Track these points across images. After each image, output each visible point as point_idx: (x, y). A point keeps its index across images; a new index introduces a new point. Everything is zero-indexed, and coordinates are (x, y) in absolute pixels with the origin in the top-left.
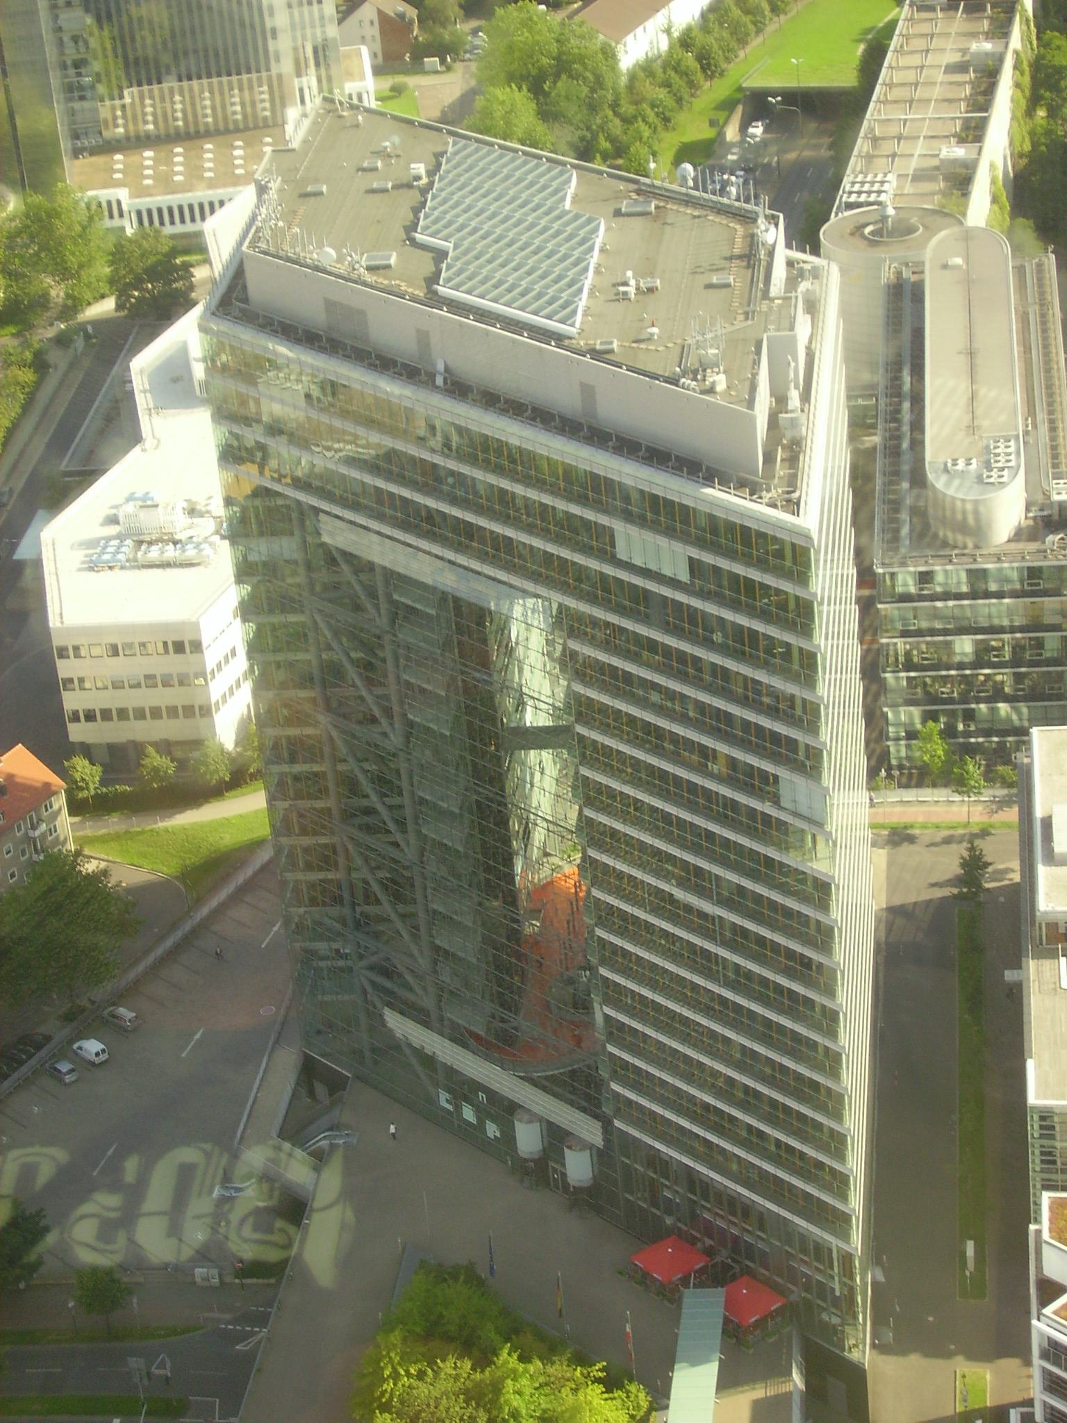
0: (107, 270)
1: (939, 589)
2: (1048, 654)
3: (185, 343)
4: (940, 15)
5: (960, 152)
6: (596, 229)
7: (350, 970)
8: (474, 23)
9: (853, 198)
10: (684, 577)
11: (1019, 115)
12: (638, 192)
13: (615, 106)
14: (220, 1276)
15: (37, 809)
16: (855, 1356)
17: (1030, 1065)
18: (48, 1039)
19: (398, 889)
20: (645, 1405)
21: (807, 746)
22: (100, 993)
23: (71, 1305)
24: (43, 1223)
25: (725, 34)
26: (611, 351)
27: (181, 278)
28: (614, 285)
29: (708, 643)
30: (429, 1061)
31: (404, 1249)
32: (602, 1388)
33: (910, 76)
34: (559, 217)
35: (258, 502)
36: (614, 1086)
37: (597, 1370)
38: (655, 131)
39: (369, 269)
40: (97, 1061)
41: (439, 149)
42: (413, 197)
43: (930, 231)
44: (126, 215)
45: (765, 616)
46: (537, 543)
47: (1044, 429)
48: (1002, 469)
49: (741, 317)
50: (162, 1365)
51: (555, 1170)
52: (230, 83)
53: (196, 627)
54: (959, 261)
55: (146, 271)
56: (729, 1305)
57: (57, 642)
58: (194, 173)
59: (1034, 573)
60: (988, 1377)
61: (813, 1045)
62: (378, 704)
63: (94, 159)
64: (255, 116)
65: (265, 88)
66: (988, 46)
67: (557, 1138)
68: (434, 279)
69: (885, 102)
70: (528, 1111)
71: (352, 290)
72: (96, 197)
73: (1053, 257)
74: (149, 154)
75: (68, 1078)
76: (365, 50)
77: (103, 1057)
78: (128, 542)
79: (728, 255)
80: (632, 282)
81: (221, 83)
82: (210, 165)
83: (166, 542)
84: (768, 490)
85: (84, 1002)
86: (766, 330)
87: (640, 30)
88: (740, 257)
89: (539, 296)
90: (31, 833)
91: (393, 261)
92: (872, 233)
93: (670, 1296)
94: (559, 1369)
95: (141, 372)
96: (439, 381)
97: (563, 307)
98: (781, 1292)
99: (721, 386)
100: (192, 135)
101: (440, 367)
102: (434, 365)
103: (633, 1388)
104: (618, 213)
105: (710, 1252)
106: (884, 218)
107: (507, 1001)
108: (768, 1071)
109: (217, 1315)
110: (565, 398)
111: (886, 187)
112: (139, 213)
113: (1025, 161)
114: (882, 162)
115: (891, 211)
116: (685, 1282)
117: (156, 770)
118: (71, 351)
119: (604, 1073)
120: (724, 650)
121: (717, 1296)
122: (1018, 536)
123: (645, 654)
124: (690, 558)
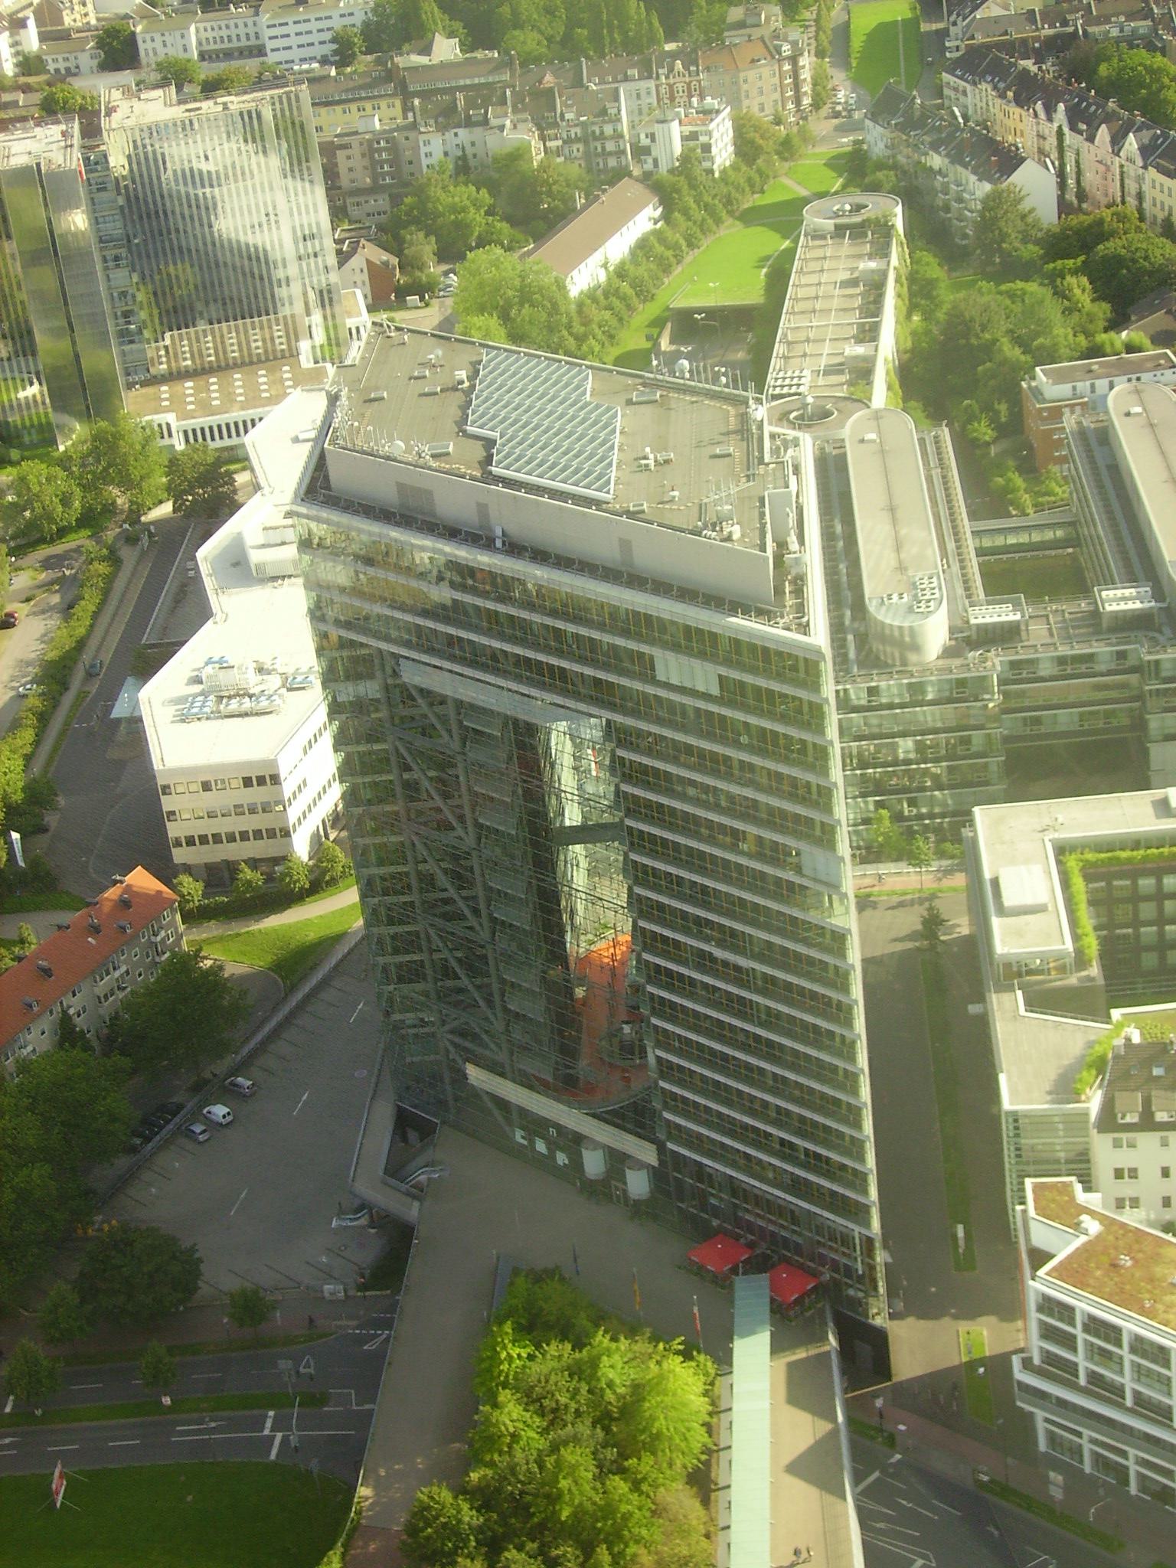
0: (164, 480)
1: (884, 701)
2: (974, 749)
3: (240, 534)
4: (830, 242)
5: (860, 350)
6: (615, 416)
7: (433, 1035)
8: (445, 267)
9: (778, 391)
10: (715, 691)
11: (901, 319)
12: (644, 385)
13: (569, 327)
14: (345, 1291)
15: (158, 919)
16: (878, 1321)
17: (1002, 1078)
18: (180, 1107)
19: (475, 964)
20: (712, 1372)
21: (822, 823)
22: (222, 1066)
23: (225, 1320)
24: (197, 1255)
25: (652, 266)
26: (643, 512)
27: (226, 483)
28: (636, 459)
29: (737, 745)
30: (503, 1104)
31: (498, 1258)
32: (681, 1359)
33: (811, 292)
34: (582, 408)
35: (345, 653)
36: (667, 1115)
37: (677, 1344)
38: (603, 345)
39: (433, 456)
40: (224, 1122)
41: (474, 359)
42: (459, 398)
43: (845, 415)
44: (174, 433)
45: (783, 718)
46: (588, 671)
47: (956, 568)
48: (929, 601)
49: (744, 480)
50: (307, 1366)
51: (617, 1189)
52: (180, 335)
53: (273, 763)
54: (872, 436)
55: (197, 480)
56: (774, 1288)
57: (160, 782)
58: (229, 399)
59: (961, 683)
60: (985, 1333)
61: (834, 1069)
62: (453, 812)
63: (144, 390)
64: (274, 351)
65: (210, 338)
66: (873, 265)
67: (618, 1161)
68: (489, 460)
69: (793, 313)
70: (593, 1141)
71: (421, 474)
72: (150, 423)
73: (946, 430)
74: (189, 384)
75: (201, 1138)
76: (359, 293)
77: (229, 1119)
78: (212, 697)
79: (724, 430)
80: (651, 456)
81: (244, 324)
82: (241, 391)
83: (243, 695)
84: (782, 617)
85: (207, 1075)
86: (765, 488)
87: (582, 266)
88: (735, 432)
89: (576, 472)
90: (153, 938)
91: (451, 449)
92: (796, 418)
93: (723, 1283)
94: (642, 1346)
95: (206, 559)
96: (499, 544)
97: (598, 479)
98: (815, 1275)
99: (737, 535)
100: (222, 367)
101: (499, 532)
102: (491, 530)
103: (702, 1358)
104: (629, 402)
105: (751, 1246)
106: (805, 406)
107: (568, 1051)
108: (797, 1093)
109: (344, 1323)
110: (605, 551)
111: (803, 381)
112: (185, 432)
113: (908, 355)
114: (796, 361)
115: (810, 400)
116: (734, 1271)
117: (249, 882)
118: (138, 548)
119: (657, 1105)
120: (751, 749)
121: (763, 1280)
122: (948, 653)
123: (683, 757)
124: (720, 676)
